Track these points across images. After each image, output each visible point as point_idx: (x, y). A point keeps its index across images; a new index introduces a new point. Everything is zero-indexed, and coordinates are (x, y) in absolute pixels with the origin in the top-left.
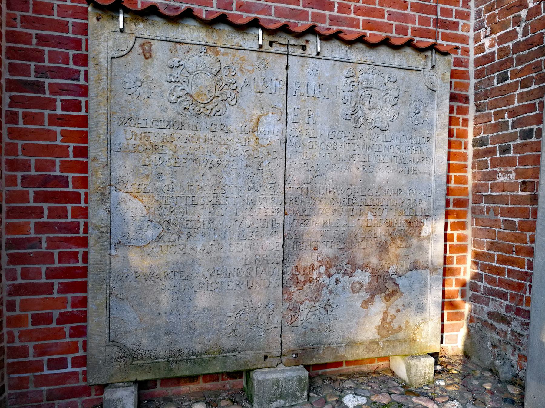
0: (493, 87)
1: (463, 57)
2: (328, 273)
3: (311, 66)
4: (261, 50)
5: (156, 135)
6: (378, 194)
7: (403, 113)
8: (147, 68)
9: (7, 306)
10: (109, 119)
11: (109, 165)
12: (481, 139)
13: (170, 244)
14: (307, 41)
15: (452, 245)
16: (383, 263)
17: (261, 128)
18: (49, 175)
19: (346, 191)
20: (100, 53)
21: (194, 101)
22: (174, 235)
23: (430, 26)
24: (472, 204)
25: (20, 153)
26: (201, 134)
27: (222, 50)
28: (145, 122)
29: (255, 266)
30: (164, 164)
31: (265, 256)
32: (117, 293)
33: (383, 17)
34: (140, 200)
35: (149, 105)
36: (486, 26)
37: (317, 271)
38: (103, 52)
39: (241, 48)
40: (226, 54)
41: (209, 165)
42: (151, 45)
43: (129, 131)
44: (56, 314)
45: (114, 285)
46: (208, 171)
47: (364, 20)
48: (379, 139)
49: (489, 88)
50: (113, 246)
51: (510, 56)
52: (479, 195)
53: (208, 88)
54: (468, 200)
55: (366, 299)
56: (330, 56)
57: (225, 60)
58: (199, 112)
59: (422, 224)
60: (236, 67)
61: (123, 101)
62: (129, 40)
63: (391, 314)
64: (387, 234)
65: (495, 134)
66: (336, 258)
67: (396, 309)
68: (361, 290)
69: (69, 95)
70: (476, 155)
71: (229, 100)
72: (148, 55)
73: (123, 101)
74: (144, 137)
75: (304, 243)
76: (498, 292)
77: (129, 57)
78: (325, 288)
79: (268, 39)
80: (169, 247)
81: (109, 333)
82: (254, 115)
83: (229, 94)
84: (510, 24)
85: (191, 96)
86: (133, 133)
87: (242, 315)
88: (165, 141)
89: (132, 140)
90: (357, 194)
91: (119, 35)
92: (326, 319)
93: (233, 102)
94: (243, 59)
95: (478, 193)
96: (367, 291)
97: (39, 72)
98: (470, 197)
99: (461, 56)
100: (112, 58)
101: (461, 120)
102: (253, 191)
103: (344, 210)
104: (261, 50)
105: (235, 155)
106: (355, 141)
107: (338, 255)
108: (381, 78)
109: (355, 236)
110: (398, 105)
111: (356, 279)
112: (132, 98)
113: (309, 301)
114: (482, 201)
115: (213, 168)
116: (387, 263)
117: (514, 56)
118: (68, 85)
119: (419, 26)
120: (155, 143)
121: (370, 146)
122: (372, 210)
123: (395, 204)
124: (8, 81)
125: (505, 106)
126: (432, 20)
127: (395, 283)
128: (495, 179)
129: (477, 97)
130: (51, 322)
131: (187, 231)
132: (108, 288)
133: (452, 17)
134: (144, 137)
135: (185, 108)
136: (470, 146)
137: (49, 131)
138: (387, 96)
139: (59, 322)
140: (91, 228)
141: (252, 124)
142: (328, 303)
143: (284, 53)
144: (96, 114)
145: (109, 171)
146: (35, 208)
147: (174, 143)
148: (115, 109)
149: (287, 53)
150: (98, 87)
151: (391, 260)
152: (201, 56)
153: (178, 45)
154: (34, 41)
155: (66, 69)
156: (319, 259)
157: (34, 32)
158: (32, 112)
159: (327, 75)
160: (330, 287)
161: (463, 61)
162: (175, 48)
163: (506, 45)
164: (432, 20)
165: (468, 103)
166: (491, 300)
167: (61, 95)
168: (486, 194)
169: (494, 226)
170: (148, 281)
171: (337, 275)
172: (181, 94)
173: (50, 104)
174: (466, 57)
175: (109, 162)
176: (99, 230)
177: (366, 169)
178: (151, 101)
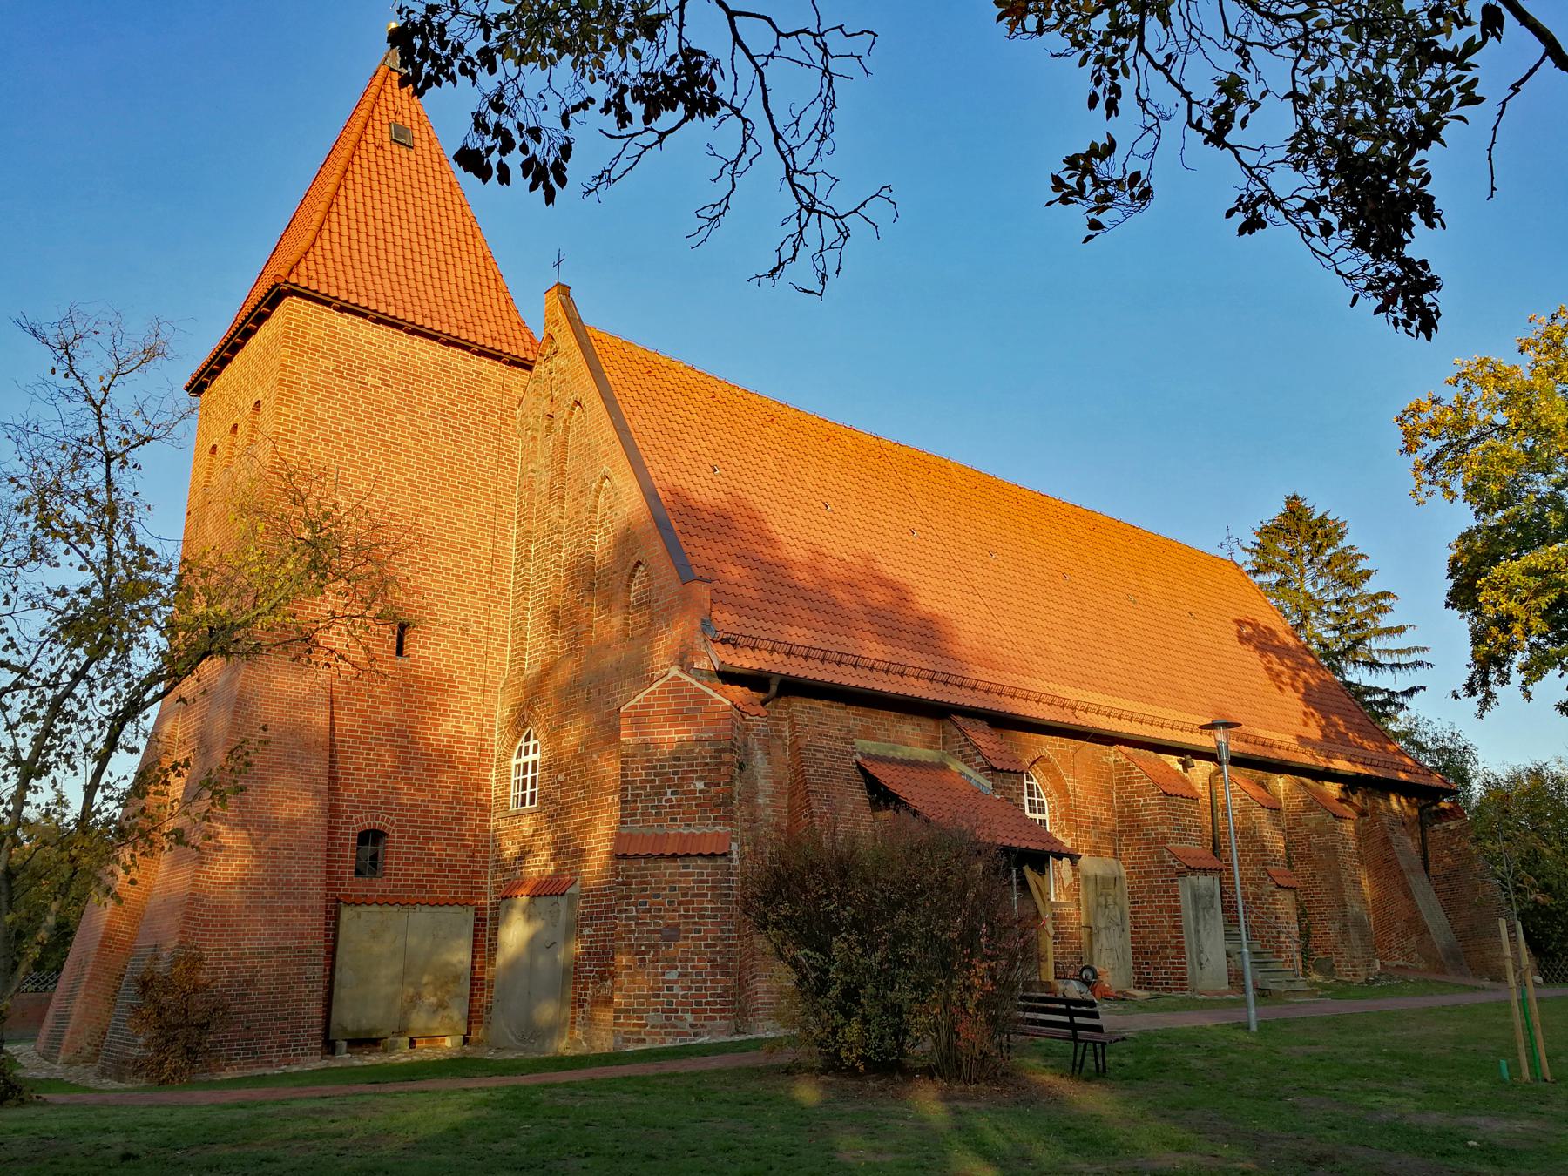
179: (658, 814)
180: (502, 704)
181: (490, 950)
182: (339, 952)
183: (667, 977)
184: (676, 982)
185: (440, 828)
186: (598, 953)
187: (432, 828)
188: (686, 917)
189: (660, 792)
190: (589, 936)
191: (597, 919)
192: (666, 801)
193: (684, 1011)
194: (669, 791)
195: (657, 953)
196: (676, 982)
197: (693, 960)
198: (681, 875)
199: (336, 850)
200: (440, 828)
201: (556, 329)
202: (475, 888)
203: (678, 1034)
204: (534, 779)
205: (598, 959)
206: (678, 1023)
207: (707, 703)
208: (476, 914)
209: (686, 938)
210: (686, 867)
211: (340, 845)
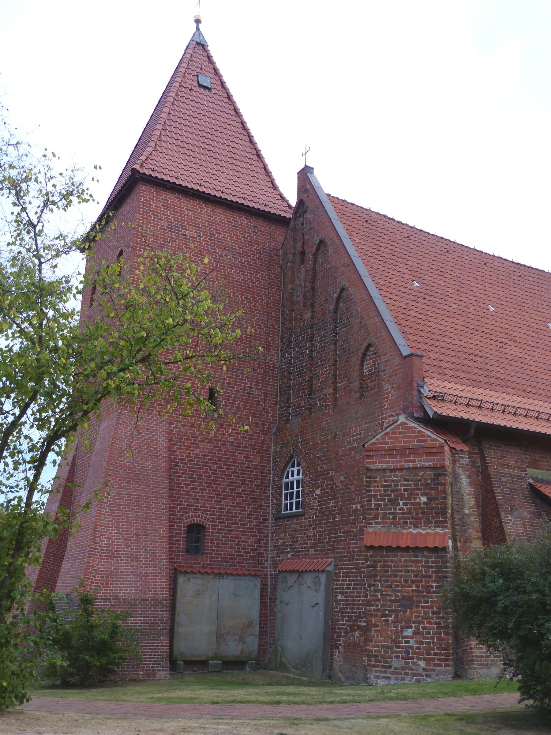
70: (270, 602)
179: (394, 518)
180: (275, 443)
181: (271, 606)
182: (178, 604)
183: (405, 634)
184: (412, 638)
185: (237, 524)
186: (348, 612)
187: (233, 524)
188: (417, 591)
189: (394, 503)
190: (341, 600)
191: (346, 589)
192: (400, 509)
193: (419, 659)
194: (401, 503)
195: (397, 616)
196: (412, 638)
197: (423, 623)
198: (412, 562)
199: (174, 537)
200: (237, 524)
201: (306, 195)
202: (261, 564)
203: (414, 675)
204: (298, 492)
205: (349, 617)
206: (414, 667)
207: (426, 441)
208: (262, 581)
209: (418, 606)
210: (416, 556)
211: (176, 533)
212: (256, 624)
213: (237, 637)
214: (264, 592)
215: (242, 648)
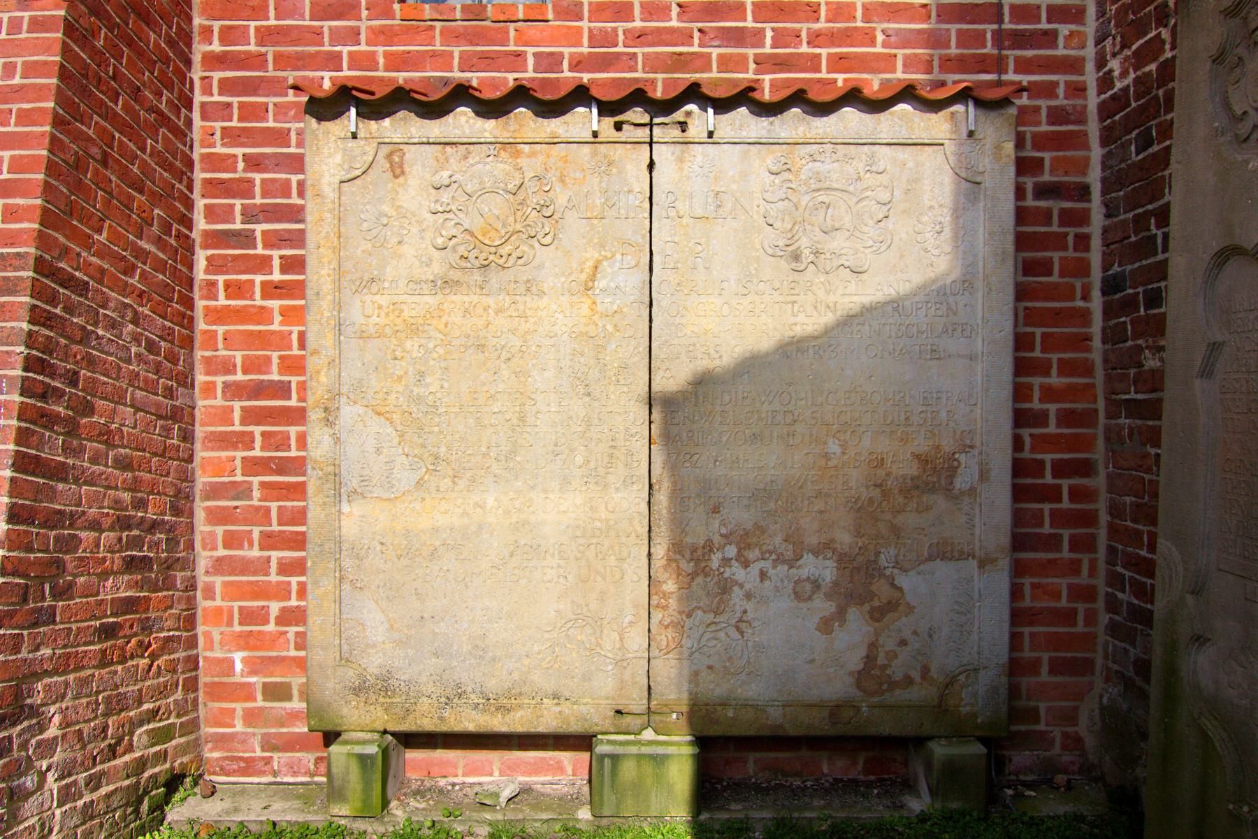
0: (1129, 162)
1: (1071, 102)
2: (743, 559)
3: (699, 159)
4: (597, 140)
5: (413, 306)
6: (849, 402)
7: (904, 236)
8: (397, 193)
9: (203, 591)
10: (337, 285)
11: (337, 360)
12: (1114, 276)
13: (440, 496)
14: (689, 114)
15: (1057, 509)
16: (864, 543)
17: (601, 284)
18: (263, 380)
19: (777, 397)
20: (322, 176)
21: (477, 242)
22: (446, 480)
23: (985, 47)
24: (1105, 421)
25: (220, 346)
26: (491, 301)
27: (527, 147)
28: (394, 285)
29: (594, 541)
30: (427, 355)
31: (611, 523)
32: (351, 577)
33: (873, 42)
34: (387, 419)
35: (400, 256)
36: (1113, 32)
37: (719, 555)
38: (326, 174)
39: (560, 140)
40: (533, 154)
41: (505, 355)
42: (404, 154)
43: (368, 301)
44: (275, 607)
45: (347, 563)
46: (503, 366)
47: (829, 55)
48: (848, 291)
49: (1123, 165)
50: (344, 497)
51: (1154, 92)
52: (1115, 400)
53: (502, 217)
54: (1096, 410)
55: (827, 614)
56: (738, 136)
57: (531, 164)
58: (486, 263)
59: (955, 463)
60: (553, 176)
61: (359, 252)
62: (367, 148)
63: (887, 649)
64: (872, 483)
65: (1136, 265)
66: (760, 529)
67: (898, 640)
68: (815, 596)
69: (292, 247)
70: (1108, 312)
71: (539, 237)
72: (398, 171)
73: (359, 252)
74: (393, 311)
75: (691, 500)
76: (210, 487)
77: (368, 178)
78: (736, 588)
79: (609, 121)
80: (437, 501)
81: (340, 645)
82: (587, 260)
83: (540, 225)
84: (1151, 24)
85: (472, 234)
86: (376, 305)
87: (571, 630)
88: (428, 316)
89: (375, 317)
90: (804, 402)
91: (351, 144)
92: (739, 648)
93: (547, 240)
94: (565, 159)
95: (1113, 397)
96: (828, 597)
97: (250, 215)
98: (1101, 405)
99: (1066, 102)
100: (341, 182)
101: (1070, 239)
102: (587, 399)
103: (775, 434)
104: (597, 140)
105: (552, 334)
106: (795, 298)
107: (762, 523)
108: (850, 169)
109: (801, 487)
110: (891, 220)
111: (804, 573)
112: (374, 246)
113: (704, 612)
114: (1121, 413)
115: (513, 360)
116: (874, 542)
117: (1161, 92)
118: (289, 231)
119: (959, 51)
120: (412, 321)
121: (828, 307)
122: (838, 435)
123: (888, 422)
124: (206, 234)
125: (1150, 203)
126: (989, 36)
127: (893, 585)
128: (1140, 365)
129: (1107, 186)
130: (266, 622)
131: (469, 474)
132: (338, 569)
133: (1039, 22)
134: (393, 311)
135: (462, 256)
136: (1096, 294)
137: (262, 308)
138: (864, 203)
139: (280, 621)
140: (309, 467)
141: (584, 277)
142: (745, 618)
143: (642, 140)
144: (316, 277)
145: (337, 370)
146: (243, 433)
147: (444, 320)
148: (348, 266)
149: (648, 140)
150: (320, 232)
151: (883, 537)
152: (487, 163)
153: (448, 148)
154: (241, 165)
155: (287, 205)
156: (724, 531)
157: (239, 151)
158: (237, 280)
159: (731, 173)
160: (747, 586)
161: (1071, 111)
162: (444, 153)
163: (1147, 69)
164: (989, 36)
165: (1089, 201)
166: (1139, 633)
167: (279, 248)
168: (1127, 397)
169: (1139, 468)
170: (402, 559)
171: (762, 564)
172: (454, 232)
173: (263, 264)
174: (1080, 102)
175: (337, 355)
176: (322, 470)
177: (821, 352)
178: (405, 249)
181: (1113, 336)
212: (984, 475)
213: (827, 571)
214: (1134, 408)
215: (873, 646)
